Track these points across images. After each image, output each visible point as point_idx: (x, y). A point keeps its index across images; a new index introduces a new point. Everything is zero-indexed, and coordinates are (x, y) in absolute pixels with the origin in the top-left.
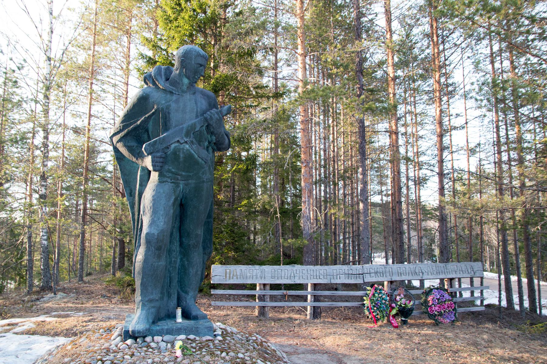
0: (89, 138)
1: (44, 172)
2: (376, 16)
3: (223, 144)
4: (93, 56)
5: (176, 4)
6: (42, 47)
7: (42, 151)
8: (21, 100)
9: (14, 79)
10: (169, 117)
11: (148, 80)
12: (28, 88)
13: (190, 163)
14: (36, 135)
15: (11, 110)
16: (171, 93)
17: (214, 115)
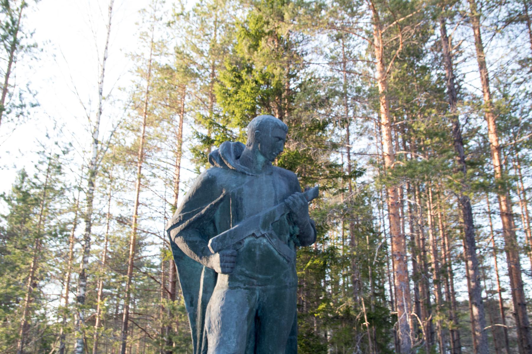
0: (136, 229)
1: (83, 270)
2: (464, 77)
3: (308, 237)
4: (143, 137)
5: (236, 77)
6: (89, 129)
7: (83, 246)
8: (64, 187)
9: (58, 165)
10: (241, 204)
11: (214, 159)
12: (73, 175)
13: (269, 264)
14: (78, 226)
15: (53, 199)
16: (243, 173)
17: (298, 200)
